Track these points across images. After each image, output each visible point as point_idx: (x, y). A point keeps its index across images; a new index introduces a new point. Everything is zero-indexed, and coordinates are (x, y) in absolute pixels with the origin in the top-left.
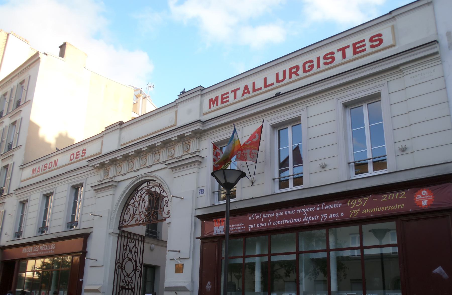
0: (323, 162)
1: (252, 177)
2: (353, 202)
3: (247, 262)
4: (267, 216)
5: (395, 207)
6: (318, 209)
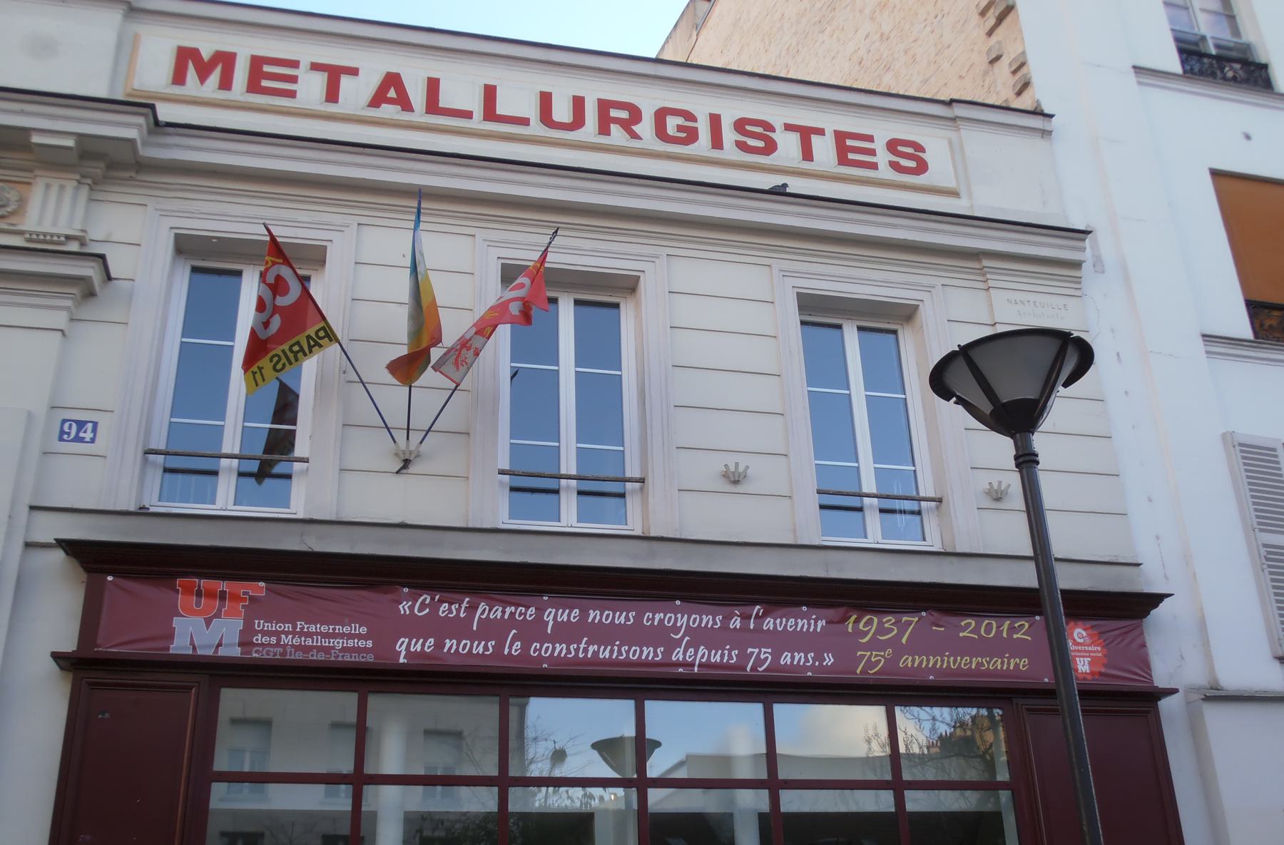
0: (744, 461)
1: (415, 437)
2: (867, 624)
3: (910, 807)
4: (497, 613)
5: (1002, 663)
6: (736, 623)
